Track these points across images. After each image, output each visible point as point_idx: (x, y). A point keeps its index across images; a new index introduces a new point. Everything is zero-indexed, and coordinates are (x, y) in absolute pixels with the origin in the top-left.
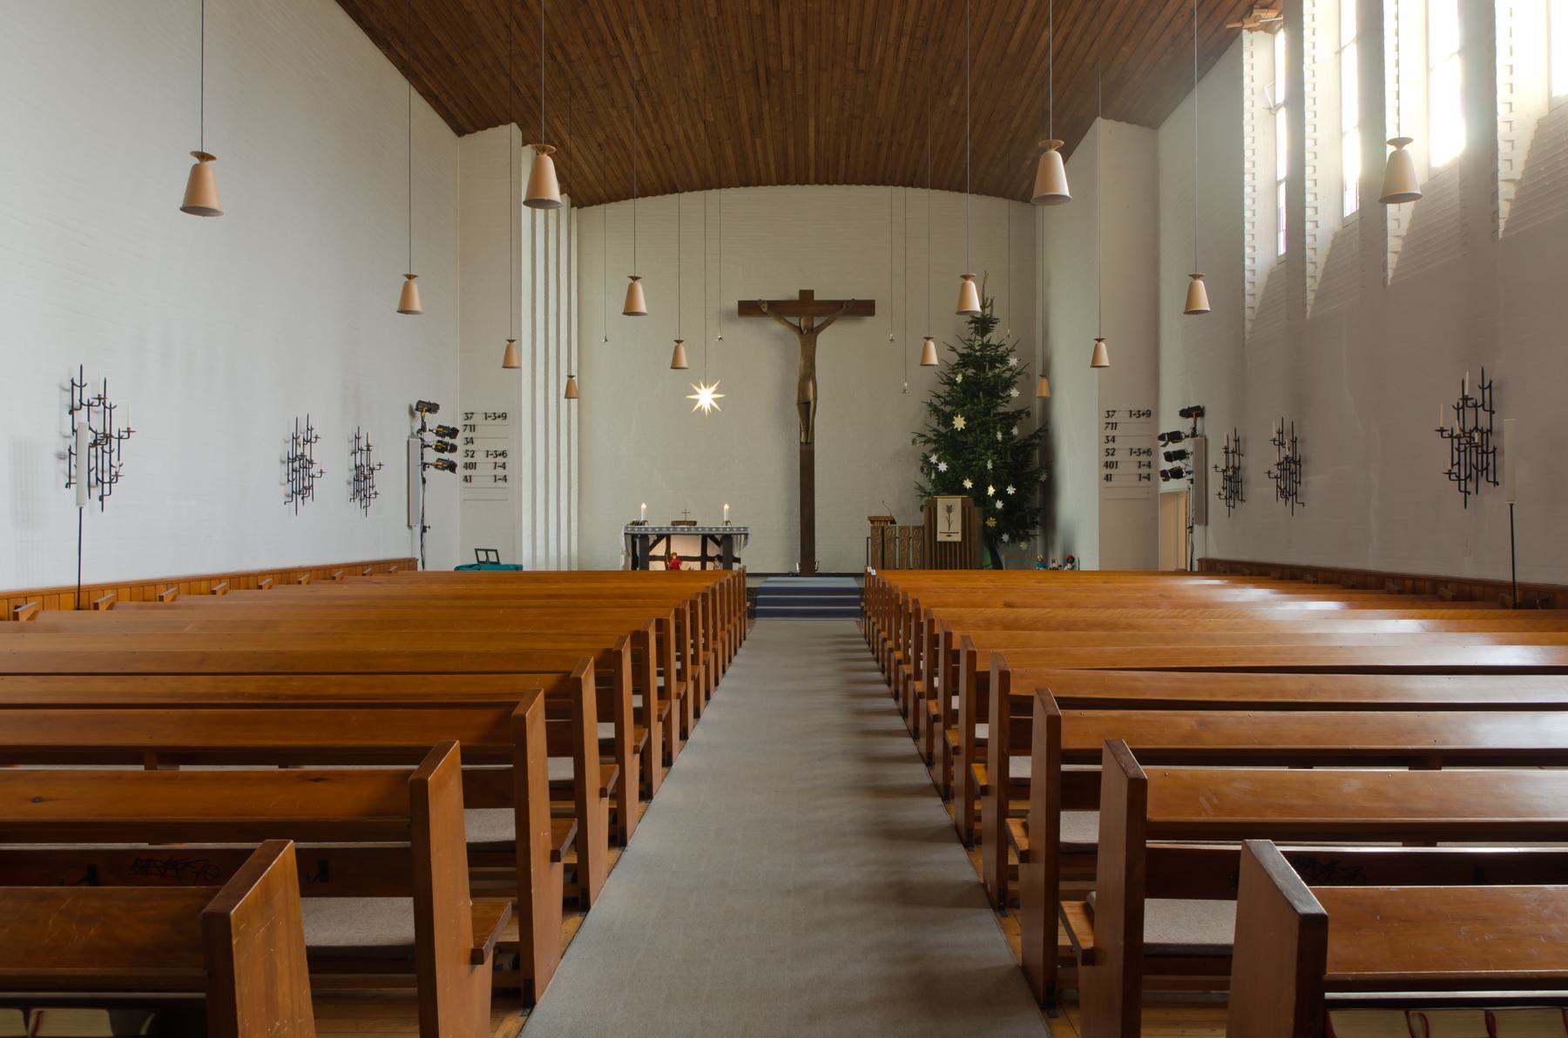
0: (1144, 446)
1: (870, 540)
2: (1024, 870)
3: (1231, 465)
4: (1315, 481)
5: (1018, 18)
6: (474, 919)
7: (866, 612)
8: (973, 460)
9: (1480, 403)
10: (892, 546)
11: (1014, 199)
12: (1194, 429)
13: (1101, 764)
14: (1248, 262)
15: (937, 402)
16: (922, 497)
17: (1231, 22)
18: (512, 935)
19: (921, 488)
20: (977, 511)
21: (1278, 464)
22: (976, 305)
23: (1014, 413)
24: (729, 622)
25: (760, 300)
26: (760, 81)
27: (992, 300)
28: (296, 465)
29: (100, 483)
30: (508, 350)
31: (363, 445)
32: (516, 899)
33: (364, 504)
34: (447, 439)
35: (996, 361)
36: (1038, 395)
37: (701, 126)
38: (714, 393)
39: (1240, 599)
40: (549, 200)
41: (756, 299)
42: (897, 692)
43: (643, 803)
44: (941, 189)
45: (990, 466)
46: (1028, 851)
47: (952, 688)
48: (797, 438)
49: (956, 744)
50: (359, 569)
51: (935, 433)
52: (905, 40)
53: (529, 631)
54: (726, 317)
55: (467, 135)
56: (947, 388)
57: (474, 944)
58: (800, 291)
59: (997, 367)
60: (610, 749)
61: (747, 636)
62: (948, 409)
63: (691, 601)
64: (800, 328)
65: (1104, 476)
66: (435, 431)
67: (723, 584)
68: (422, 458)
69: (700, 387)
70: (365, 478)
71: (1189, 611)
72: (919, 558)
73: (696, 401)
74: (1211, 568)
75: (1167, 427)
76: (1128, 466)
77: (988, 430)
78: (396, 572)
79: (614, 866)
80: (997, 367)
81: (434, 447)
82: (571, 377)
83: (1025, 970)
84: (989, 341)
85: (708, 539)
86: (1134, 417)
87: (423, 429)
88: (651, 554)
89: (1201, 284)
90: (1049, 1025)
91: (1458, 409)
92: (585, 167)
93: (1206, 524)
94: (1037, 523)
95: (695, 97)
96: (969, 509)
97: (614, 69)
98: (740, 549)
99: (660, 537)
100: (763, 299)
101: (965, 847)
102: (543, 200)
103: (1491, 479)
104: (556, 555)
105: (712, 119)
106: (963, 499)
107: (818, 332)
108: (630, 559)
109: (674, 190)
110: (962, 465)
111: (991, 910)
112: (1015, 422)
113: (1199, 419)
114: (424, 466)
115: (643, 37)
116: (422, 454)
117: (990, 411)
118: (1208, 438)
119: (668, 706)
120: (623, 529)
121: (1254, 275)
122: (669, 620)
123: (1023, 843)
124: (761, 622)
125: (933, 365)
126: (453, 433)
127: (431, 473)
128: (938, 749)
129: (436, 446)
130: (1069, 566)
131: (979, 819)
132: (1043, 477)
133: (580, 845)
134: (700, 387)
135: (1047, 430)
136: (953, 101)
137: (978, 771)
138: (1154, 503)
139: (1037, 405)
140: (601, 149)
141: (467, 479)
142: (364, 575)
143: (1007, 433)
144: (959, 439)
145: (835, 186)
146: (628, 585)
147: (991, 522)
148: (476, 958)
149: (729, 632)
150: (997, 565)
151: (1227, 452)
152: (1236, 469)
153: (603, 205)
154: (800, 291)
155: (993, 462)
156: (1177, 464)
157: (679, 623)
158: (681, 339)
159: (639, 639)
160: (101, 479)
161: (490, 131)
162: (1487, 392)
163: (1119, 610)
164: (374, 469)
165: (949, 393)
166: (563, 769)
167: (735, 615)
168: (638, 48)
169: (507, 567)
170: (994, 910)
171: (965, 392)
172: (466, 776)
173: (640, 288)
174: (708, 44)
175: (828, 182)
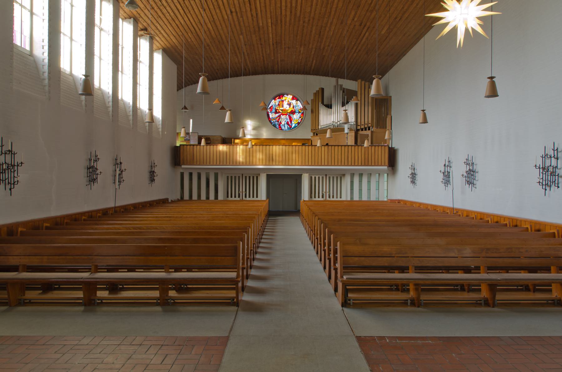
4: (479, 177)
9: (552, 156)
21: (466, 172)
28: (91, 170)
29: (10, 185)
91: (542, 157)
103: (556, 185)
152: (449, 173)
160: (10, 182)
162: (556, 152)
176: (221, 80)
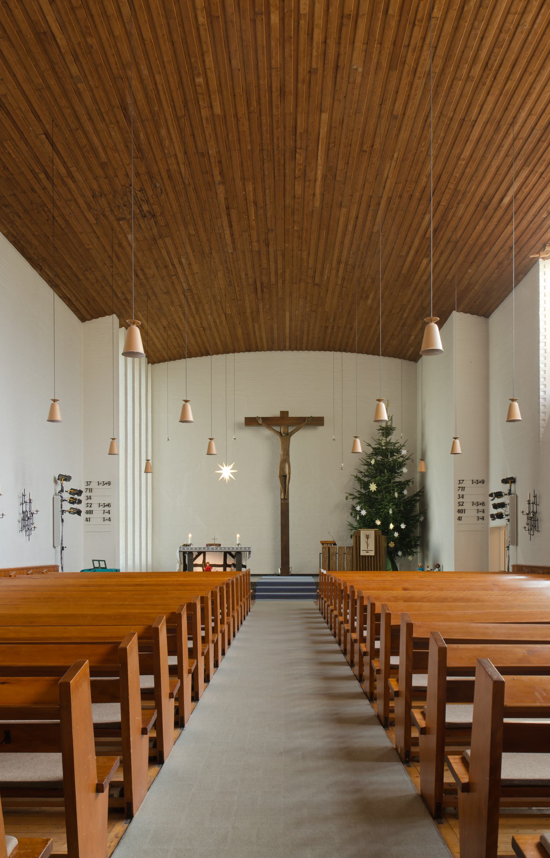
0: (480, 501)
1: (321, 554)
2: (422, 740)
3: (531, 511)
5: (408, 253)
6: (97, 766)
7: (320, 595)
8: (381, 509)
10: (334, 558)
11: (404, 359)
12: (510, 490)
13: (474, 676)
14: (542, 394)
15: (360, 475)
16: (351, 530)
17: (533, 254)
18: (120, 777)
19: (351, 525)
20: (383, 538)
22: (385, 417)
23: (404, 482)
24: (241, 601)
25: (257, 417)
26: (258, 290)
30: (112, 444)
31: (27, 499)
32: (122, 757)
33: (28, 534)
35: (394, 452)
36: (419, 470)
37: (223, 317)
38: (231, 469)
39: (539, 586)
40: (137, 353)
41: (256, 416)
42: (340, 640)
43: (194, 703)
44: (362, 353)
45: (391, 512)
46: (425, 727)
47: (375, 635)
48: (279, 496)
49: (378, 668)
50: (25, 571)
51: (359, 493)
52: (342, 266)
53: (126, 603)
54: (238, 426)
55: (87, 322)
56: (366, 467)
57: (98, 781)
59: (395, 456)
60: (175, 671)
61: (251, 610)
62: (366, 479)
63: (220, 587)
65: (457, 518)
66: (69, 492)
67: (238, 578)
68: (61, 508)
69: (223, 466)
70: (29, 519)
71: (511, 592)
72: (350, 565)
73: (221, 474)
74: (519, 570)
75: (493, 490)
76: (471, 512)
77: (389, 491)
78: (47, 573)
79: (177, 738)
80: (395, 456)
81: (68, 501)
82: (148, 460)
83: (423, 797)
84: (390, 440)
85: (228, 555)
86: (474, 484)
87: (62, 491)
88: (194, 563)
89: (516, 404)
90: (438, 828)
92: (155, 340)
93: (517, 545)
94: (418, 545)
97: (173, 283)
98: (246, 560)
99: (199, 553)
100: (259, 416)
101: (384, 727)
102: (134, 352)
104: (139, 563)
105: (230, 312)
106: (375, 532)
107: (291, 435)
109: (208, 354)
110: (375, 512)
111: (401, 763)
112: (406, 487)
113: (513, 485)
114: (63, 512)
115: (190, 264)
116: (61, 505)
117: (390, 480)
119: (207, 647)
120: (178, 549)
121: (545, 401)
122: (208, 597)
123: (422, 724)
124: (258, 602)
125: (359, 453)
126: (80, 493)
127: (66, 516)
128: (366, 672)
129: (70, 500)
130: (437, 569)
131: (393, 711)
132: (422, 519)
133: (158, 726)
134: (223, 466)
135: (423, 492)
136: (369, 302)
137: (393, 683)
138: (486, 533)
139: (418, 478)
140: (165, 330)
141: (87, 520)
142: (28, 574)
143: (401, 493)
144: (373, 496)
145: (301, 351)
146: (182, 579)
147: (392, 545)
148: (99, 789)
149: (241, 606)
150: (395, 568)
151: (529, 504)
152: (535, 513)
153: (166, 362)
155: (393, 510)
156: (500, 510)
157: (213, 599)
159: (191, 607)
161: (101, 319)
163: (471, 592)
164: (33, 513)
165: (367, 470)
166: (148, 682)
167: (244, 597)
168: (187, 272)
169: (111, 570)
170: (403, 763)
171: (376, 470)
172: (93, 683)
173: (189, 407)
174: (227, 268)
175: (296, 349)
176: (231, 354)
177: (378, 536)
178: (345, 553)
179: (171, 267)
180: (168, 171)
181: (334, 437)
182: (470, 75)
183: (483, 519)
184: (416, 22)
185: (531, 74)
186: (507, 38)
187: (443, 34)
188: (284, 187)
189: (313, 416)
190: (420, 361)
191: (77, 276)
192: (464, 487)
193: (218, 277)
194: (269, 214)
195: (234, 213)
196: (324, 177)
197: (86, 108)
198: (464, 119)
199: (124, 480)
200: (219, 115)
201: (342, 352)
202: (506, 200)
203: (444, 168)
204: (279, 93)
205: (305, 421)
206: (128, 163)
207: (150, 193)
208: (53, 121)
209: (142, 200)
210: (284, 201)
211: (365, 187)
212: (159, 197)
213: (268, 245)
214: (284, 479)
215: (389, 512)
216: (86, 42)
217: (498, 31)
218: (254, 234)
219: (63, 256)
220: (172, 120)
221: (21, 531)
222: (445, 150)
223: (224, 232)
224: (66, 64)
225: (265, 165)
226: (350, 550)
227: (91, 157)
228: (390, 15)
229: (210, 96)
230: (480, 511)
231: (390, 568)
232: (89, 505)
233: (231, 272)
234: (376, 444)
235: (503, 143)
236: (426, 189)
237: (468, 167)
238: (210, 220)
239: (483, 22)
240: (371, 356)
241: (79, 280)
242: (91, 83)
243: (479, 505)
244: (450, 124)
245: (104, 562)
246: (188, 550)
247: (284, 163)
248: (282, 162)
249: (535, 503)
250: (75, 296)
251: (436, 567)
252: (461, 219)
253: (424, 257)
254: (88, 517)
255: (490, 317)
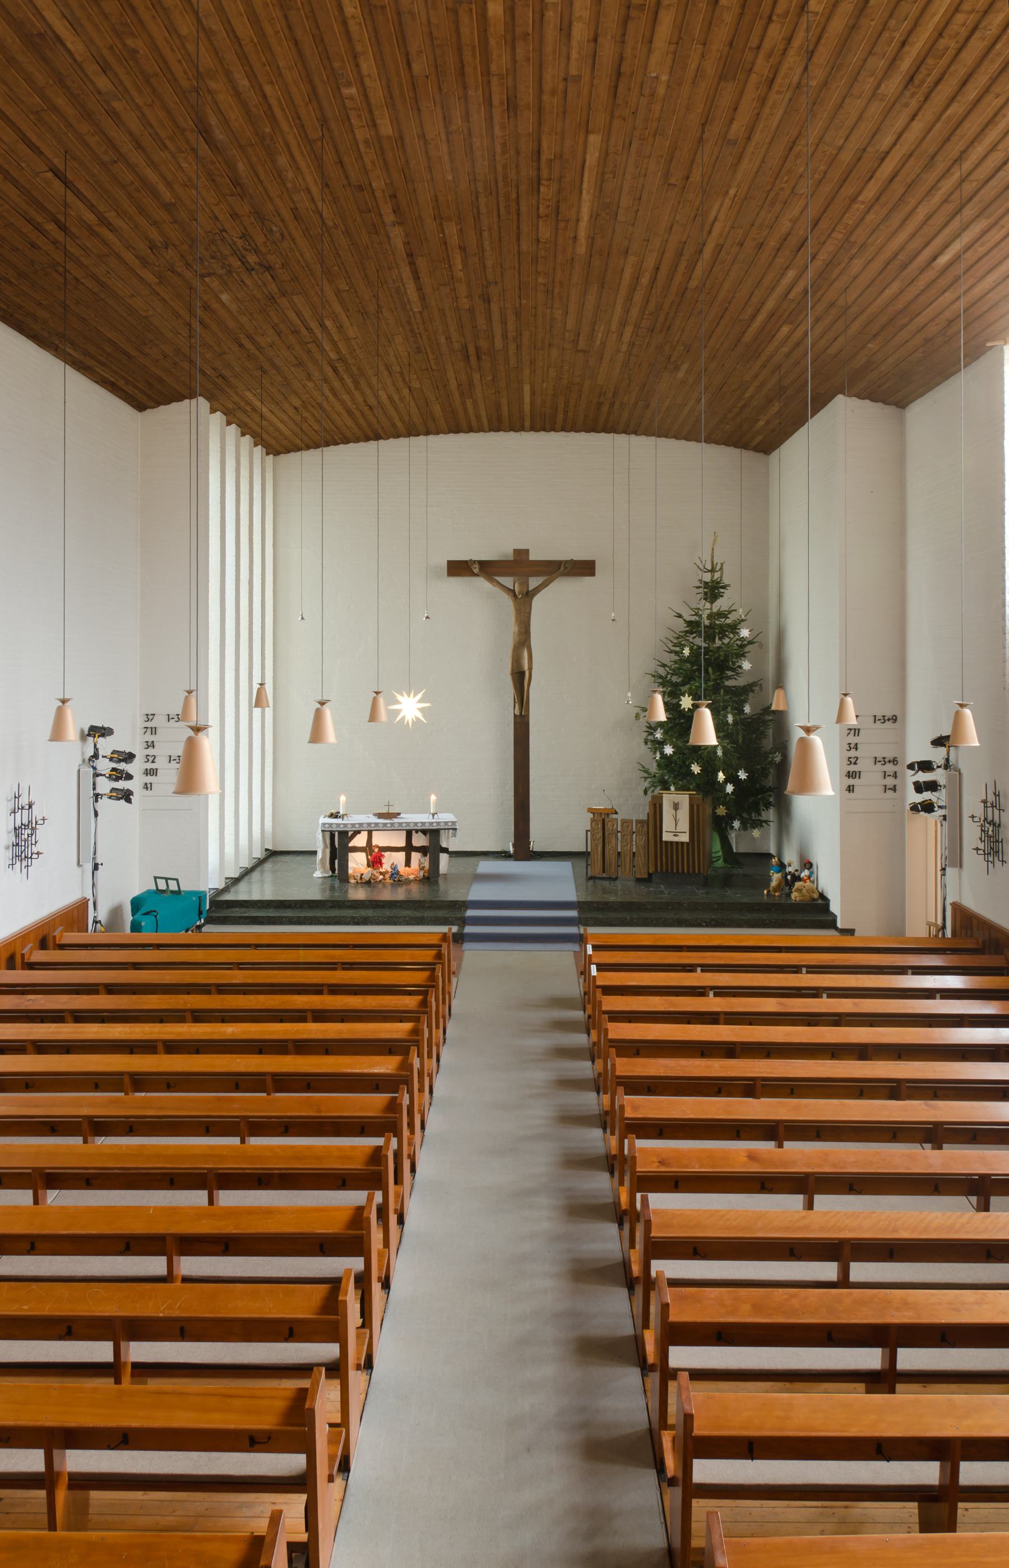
0: (889, 755)
1: (589, 833)
5: (754, 317)
10: (614, 842)
12: (947, 760)
16: (646, 778)
25: (471, 560)
27: (722, 564)
34: (122, 766)
37: (406, 392)
41: (467, 559)
44: (666, 437)
48: (509, 711)
52: (628, 330)
55: (149, 410)
58: (514, 550)
64: (514, 591)
68: (94, 789)
72: (642, 855)
76: (872, 776)
87: (96, 756)
88: (350, 845)
93: (961, 866)
95: (398, 369)
96: (698, 806)
98: (448, 838)
104: (247, 844)
107: (534, 595)
108: (328, 851)
109: (377, 437)
114: (97, 797)
115: (340, 328)
116: (94, 784)
118: (962, 771)
126: (129, 757)
127: (104, 804)
136: (681, 375)
154: (514, 550)
156: (927, 795)
158: (380, 690)
161: (174, 406)
173: (328, 713)
174: (412, 331)
177: (695, 806)
178: (634, 832)
179: (304, 331)
180: (295, 210)
181: (613, 615)
182: (879, 91)
183: (895, 791)
184: (774, 18)
185: (998, 96)
186: (953, 45)
187: (826, 35)
188: (518, 228)
189: (575, 559)
190: (776, 453)
191: (126, 353)
192: (859, 729)
193: (395, 342)
194: (489, 263)
195: (422, 263)
196: (594, 217)
197: (130, 133)
198: (865, 149)
199: (218, 702)
200: (389, 137)
201: (629, 434)
202: (943, 260)
203: (824, 211)
204: (506, 108)
205: (560, 568)
206: (216, 202)
207: (260, 239)
208: (66, 152)
209: (246, 250)
210: (519, 246)
211: (673, 231)
212: (279, 244)
213: (488, 301)
214: (520, 679)
215: (717, 753)
216: (125, 45)
217: (936, 34)
218: (462, 289)
219: (99, 328)
220: (299, 144)
221: (11, 866)
222: (826, 189)
223: (404, 286)
224: (87, 75)
225: (480, 200)
226: (643, 827)
227: (144, 197)
228: (722, 6)
229: (370, 111)
230: (890, 776)
231: (717, 850)
232: (151, 759)
233: (418, 336)
234: (692, 615)
235: (940, 185)
236: (790, 237)
237: (871, 213)
238: (378, 271)
239: (906, 23)
240: (683, 442)
241: (130, 357)
242: (137, 101)
243: (887, 764)
244: (837, 155)
245: (175, 882)
246: (338, 829)
247: (518, 197)
248: (514, 196)
249: (996, 806)
250: (124, 378)
251: (805, 868)
252: (855, 278)
253: (783, 323)
254: (148, 782)
255: (908, 409)
